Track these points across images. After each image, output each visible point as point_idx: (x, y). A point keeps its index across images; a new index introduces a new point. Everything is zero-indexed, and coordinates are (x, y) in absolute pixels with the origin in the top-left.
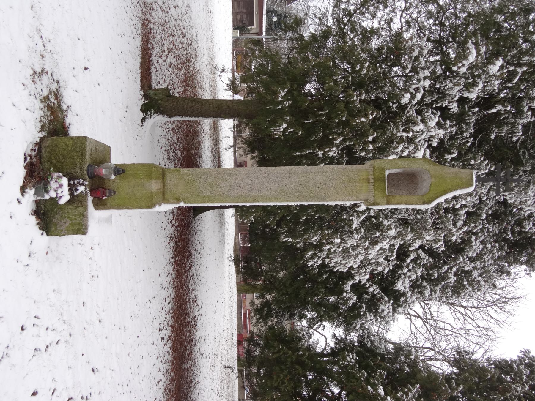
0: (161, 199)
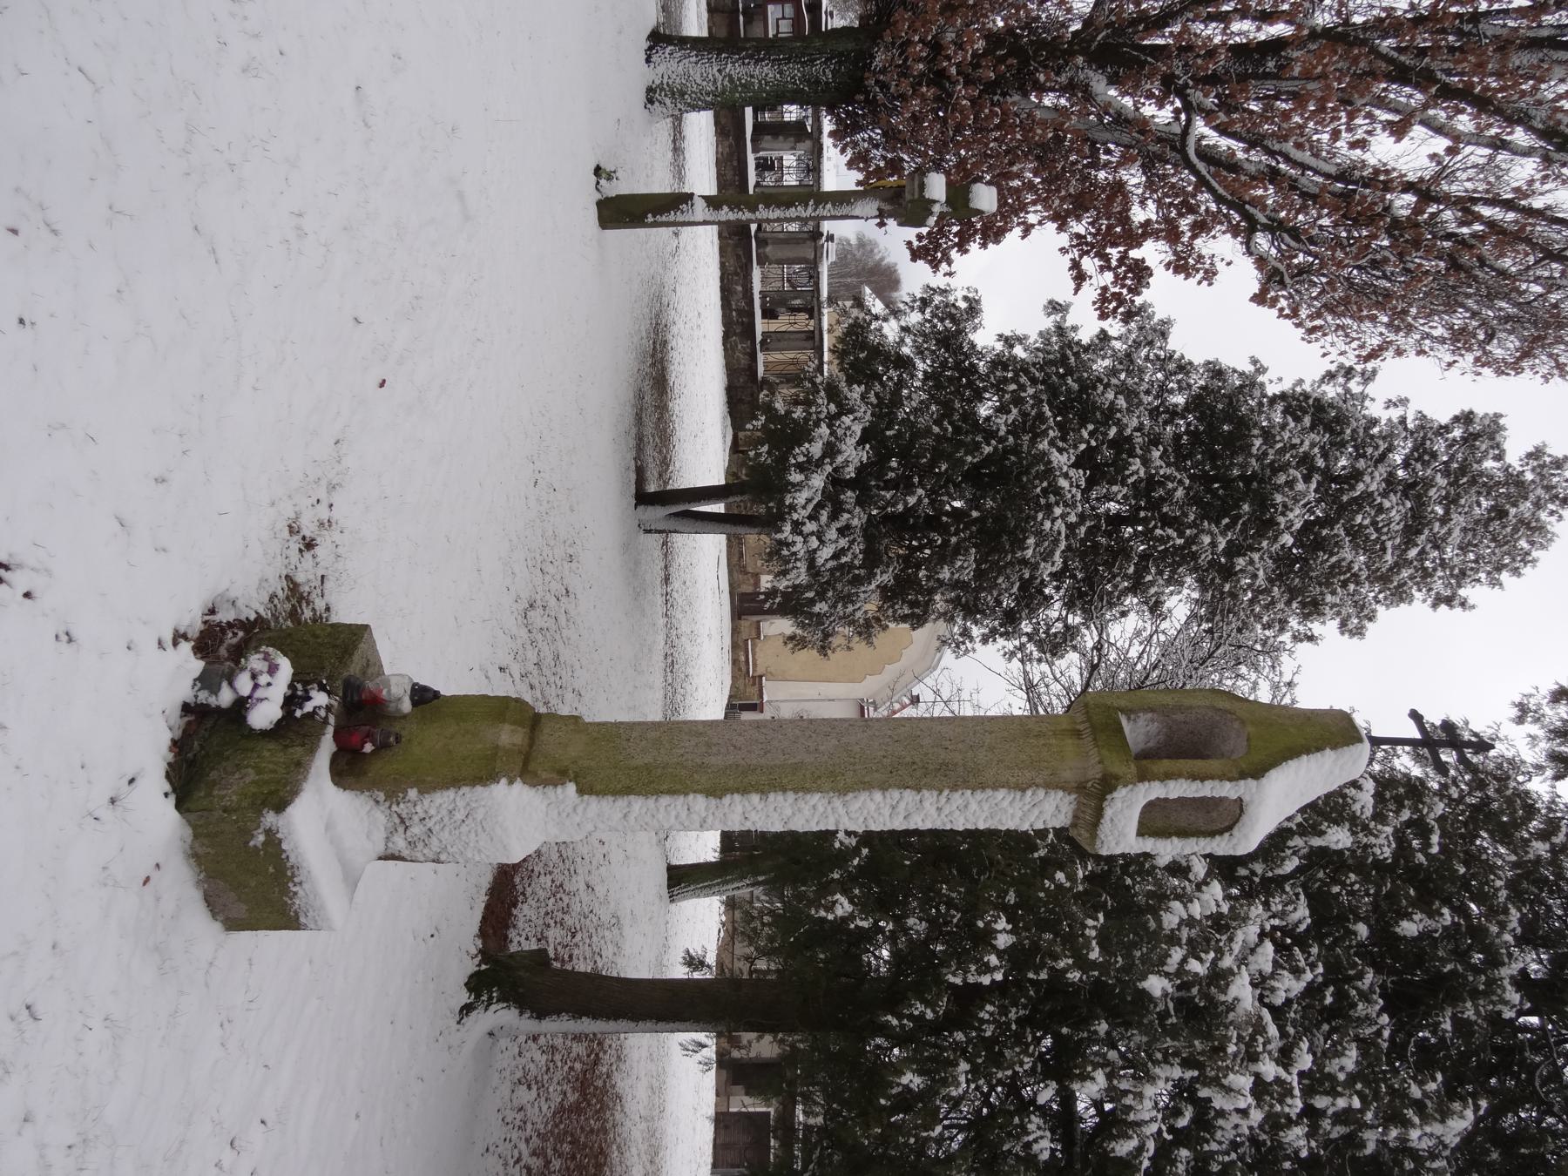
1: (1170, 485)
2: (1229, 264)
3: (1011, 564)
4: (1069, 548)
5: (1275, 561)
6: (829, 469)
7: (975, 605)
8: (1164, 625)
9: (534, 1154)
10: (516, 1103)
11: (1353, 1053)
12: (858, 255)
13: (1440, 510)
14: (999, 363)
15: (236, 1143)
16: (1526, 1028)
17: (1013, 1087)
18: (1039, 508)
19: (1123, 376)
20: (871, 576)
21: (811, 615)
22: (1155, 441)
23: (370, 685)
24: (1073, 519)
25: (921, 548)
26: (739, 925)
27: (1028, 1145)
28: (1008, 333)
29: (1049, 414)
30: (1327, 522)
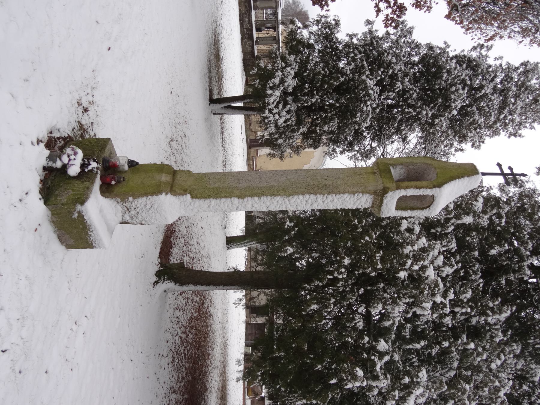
0: (169, 189)
1: (412, 92)
2: (437, 4)
3: (351, 123)
4: (372, 117)
5: (450, 121)
6: (282, 88)
7: (337, 140)
8: (407, 146)
9: (182, 332)
10: (175, 316)
11: (470, 292)
12: (293, 7)
13: (513, 100)
14: (347, 45)
15: (77, 323)
16: (532, 283)
17: (350, 306)
18: (361, 101)
19: (394, 50)
20: (299, 129)
21: (276, 145)
22: (406, 75)
23: (112, 160)
24: (374, 106)
25: (317, 119)
26: (252, 259)
27: (356, 324)
28: (351, 33)
29: (366, 65)
30: (470, 105)
